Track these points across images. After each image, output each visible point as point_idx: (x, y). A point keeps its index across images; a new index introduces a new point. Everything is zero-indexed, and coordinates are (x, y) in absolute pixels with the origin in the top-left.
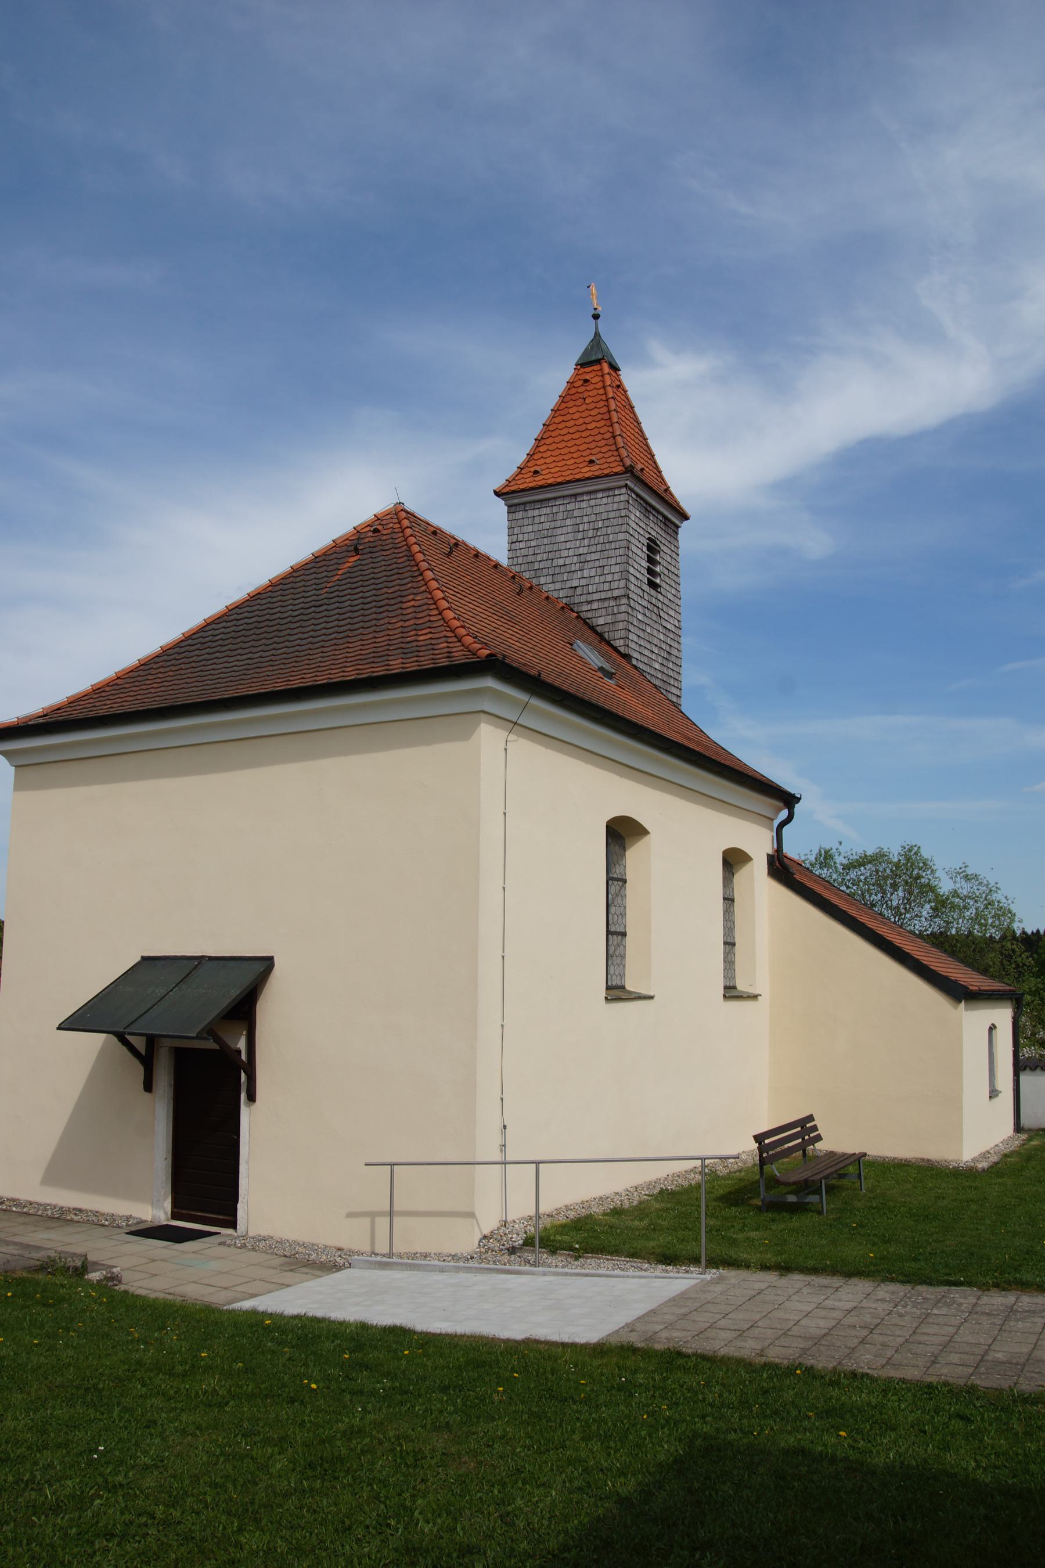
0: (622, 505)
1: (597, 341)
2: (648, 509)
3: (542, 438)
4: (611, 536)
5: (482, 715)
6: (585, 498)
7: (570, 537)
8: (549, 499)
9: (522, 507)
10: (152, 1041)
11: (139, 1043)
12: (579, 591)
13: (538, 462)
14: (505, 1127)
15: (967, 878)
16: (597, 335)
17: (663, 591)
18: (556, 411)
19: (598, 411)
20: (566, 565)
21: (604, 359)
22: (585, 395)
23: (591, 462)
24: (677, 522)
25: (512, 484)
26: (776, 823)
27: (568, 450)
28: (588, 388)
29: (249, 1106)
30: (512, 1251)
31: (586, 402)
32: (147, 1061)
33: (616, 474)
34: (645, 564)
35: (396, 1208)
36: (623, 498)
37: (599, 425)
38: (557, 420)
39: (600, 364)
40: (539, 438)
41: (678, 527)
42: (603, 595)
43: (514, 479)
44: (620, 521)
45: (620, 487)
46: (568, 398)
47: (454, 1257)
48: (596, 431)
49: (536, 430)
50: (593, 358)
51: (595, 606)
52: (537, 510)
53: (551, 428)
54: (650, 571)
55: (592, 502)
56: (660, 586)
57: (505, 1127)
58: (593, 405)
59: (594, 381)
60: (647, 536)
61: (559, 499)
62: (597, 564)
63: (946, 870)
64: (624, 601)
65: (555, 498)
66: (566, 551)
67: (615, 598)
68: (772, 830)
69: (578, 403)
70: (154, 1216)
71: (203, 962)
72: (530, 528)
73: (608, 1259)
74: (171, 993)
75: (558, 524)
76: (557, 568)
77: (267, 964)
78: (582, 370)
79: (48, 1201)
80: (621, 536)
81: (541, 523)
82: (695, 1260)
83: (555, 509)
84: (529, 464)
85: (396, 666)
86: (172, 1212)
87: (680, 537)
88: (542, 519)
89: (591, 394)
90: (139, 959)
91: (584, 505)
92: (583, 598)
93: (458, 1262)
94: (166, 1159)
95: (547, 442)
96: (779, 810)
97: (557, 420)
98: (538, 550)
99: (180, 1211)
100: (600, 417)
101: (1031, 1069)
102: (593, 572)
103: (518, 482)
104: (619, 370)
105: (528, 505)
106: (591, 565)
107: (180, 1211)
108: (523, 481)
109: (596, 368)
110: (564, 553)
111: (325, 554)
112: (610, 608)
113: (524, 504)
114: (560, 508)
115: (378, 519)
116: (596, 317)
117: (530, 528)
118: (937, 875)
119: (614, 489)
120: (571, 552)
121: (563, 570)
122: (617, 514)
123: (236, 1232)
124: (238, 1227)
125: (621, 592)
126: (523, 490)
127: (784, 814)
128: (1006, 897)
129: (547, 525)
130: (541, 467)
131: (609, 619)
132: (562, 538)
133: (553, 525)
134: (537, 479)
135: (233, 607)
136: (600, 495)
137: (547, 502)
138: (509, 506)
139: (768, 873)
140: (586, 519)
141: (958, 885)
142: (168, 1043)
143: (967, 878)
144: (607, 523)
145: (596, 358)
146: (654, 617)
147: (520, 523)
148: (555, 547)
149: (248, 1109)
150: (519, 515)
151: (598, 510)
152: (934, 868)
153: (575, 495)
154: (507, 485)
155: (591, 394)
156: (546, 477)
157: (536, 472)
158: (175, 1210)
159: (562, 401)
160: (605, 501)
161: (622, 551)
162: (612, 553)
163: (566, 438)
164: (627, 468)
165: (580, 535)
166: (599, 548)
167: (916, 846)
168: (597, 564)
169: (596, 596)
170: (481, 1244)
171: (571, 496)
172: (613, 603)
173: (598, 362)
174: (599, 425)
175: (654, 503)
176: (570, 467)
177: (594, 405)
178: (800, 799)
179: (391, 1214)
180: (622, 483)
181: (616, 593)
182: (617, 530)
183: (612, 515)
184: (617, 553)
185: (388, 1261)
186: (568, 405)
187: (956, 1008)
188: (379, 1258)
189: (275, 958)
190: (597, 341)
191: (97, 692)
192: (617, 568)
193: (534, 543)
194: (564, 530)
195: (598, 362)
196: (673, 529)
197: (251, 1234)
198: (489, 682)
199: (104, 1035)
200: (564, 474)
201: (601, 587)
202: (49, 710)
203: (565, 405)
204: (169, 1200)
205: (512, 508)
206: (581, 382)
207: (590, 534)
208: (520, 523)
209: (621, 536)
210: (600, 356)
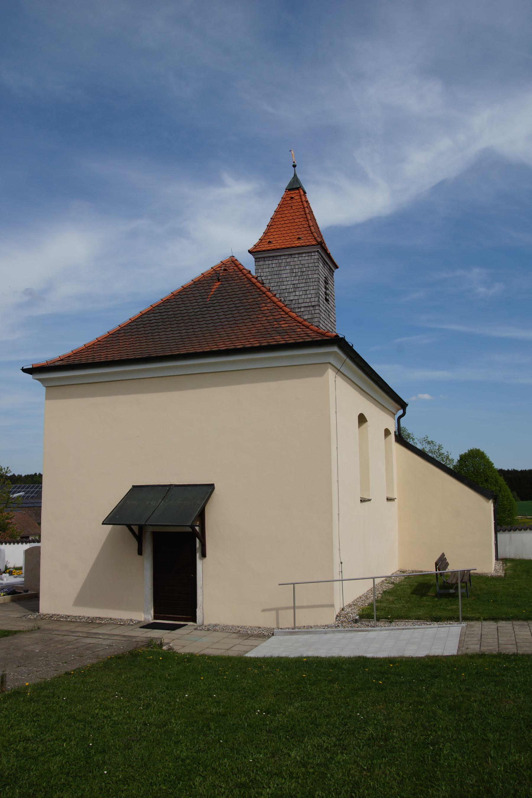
0: (315, 261)
1: (295, 179)
2: (325, 263)
3: (271, 225)
4: (310, 276)
5: (329, 365)
6: (296, 256)
7: (289, 275)
8: (277, 256)
9: (263, 259)
10: (141, 528)
11: (136, 529)
12: (294, 302)
13: (270, 237)
14: (341, 563)
15: (429, 443)
16: (295, 175)
17: (330, 303)
18: (277, 212)
19: (300, 213)
20: (287, 289)
21: (300, 187)
22: (293, 205)
23: (299, 238)
24: (334, 270)
25: (257, 247)
26: (397, 416)
27: (285, 232)
28: (293, 201)
29: (202, 560)
30: (356, 621)
31: (293, 208)
32: (139, 538)
33: (313, 245)
34: (324, 290)
35: (296, 605)
36: (316, 257)
37: (301, 220)
38: (278, 216)
39: (299, 190)
40: (269, 225)
41: (334, 272)
42: (307, 305)
43: (258, 245)
44: (315, 268)
45: (314, 252)
46: (283, 206)
47: (327, 626)
48: (300, 223)
49: (268, 221)
50: (295, 187)
51: (302, 309)
52: (271, 261)
53: (275, 220)
54: (326, 293)
55: (300, 259)
56: (329, 301)
57: (341, 563)
58: (297, 210)
59: (296, 198)
60: (325, 276)
61: (282, 256)
62: (303, 289)
63: (418, 439)
64: (317, 308)
65: (280, 256)
66: (287, 282)
67: (313, 306)
68: (394, 419)
69: (288, 209)
70: (145, 619)
71: (171, 487)
72: (267, 270)
73: (406, 622)
74: (161, 504)
75: (282, 268)
76: (282, 290)
77: (211, 487)
78: (289, 193)
79: (78, 615)
80: (316, 276)
81: (273, 267)
82: (457, 619)
83: (280, 261)
84: (265, 238)
85: (280, 340)
86: (154, 615)
87: (334, 277)
88: (274, 266)
89: (295, 204)
90: (131, 487)
91: (296, 259)
92: (296, 306)
93: (327, 628)
94: (151, 589)
95: (274, 227)
96: (398, 410)
97: (278, 216)
98: (271, 281)
99: (159, 615)
100: (301, 216)
101: (524, 530)
102: (301, 293)
103: (261, 247)
104: (306, 193)
105: (266, 258)
106: (300, 289)
107: (159, 615)
108: (263, 246)
109: (297, 191)
110: (286, 283)
111: (199, 280)
112: (311, 311)
113: (264, 258)
114: (283, 261)
115: (224, 264)
116: (294, 166)
117: (267, 270)
118: (415, 441)
119: (311, 252)
120: (289, 283)
121: (285, 291)
122: (313, 265)
123: (196, 623)
124: (197, 621)
125: (316, 303)
126: (264, 251)
127: (401, 412)
128: (447, 452)
129: (276, 269)
130: (272, 239)
131: (310, 316)
132: (284, 276)
133: (279, 269)
134: (271, 245)
135: (155, 306)
136: (304, 255)
137: (276, 257)
138: (255, 258)
139: (395, 441)
140: (297, 267)
141: (424, 446)
142: (150, 529)
143: (429, 443)
144: (308, 269)
145: (296, 187)
146: (328, 316)
147: (262, 267)
148: (281, 280)
149: (201, 561)
150: (261, 263)
151: (303, 262)
152: (414, 438)
153: (291, 255)
154: (255, 248)
155: (295, 204)
156: (276, 245)
157: (270, 242)
158: (156, 615)
159: (280, 207)
160: (307, 258)
161: (316, 283)
162: (311, 284)
163: (284, 226)
164: (319, 242)
165: (294, 275)
166: (304, 281)
167: (404, 427)
168: (303, 289)
169: (303, 305)
170: (337, 619)
171: (289, 255)
172: (311, 309)
173: (298, 189)
174: (301, 220)
175: (327, 260)
176: (288, 241)
177: (297, 210)
178: (408, 405)
179: (294, 608)
180: (316, 250)
181: (313, 304)
182: (313, 272)
183: (310, 265)
184: (314, 284)
185: (294, 630)
186: (284, 209)
187: (488, 502)
188: (290, 630)
189: (215, 485)
190: (295, 179)
191: (88, 348)
192: (313, 292)
193: (269, 277)
194: (285, 272)
195: (298, 189)
196: (332, 272)
197: (206, 623)
198: (335, 349)
199: (112, 526)
200: (285, 244)
201: (305, 300)
202: (64, 357)
203: (281, 209)
204: (153, 610)
205: (257, 260)
206: (289, 199)
207: (299, 274)
208: (262, 267)
209: (316, 276)
210: (298, 186)
